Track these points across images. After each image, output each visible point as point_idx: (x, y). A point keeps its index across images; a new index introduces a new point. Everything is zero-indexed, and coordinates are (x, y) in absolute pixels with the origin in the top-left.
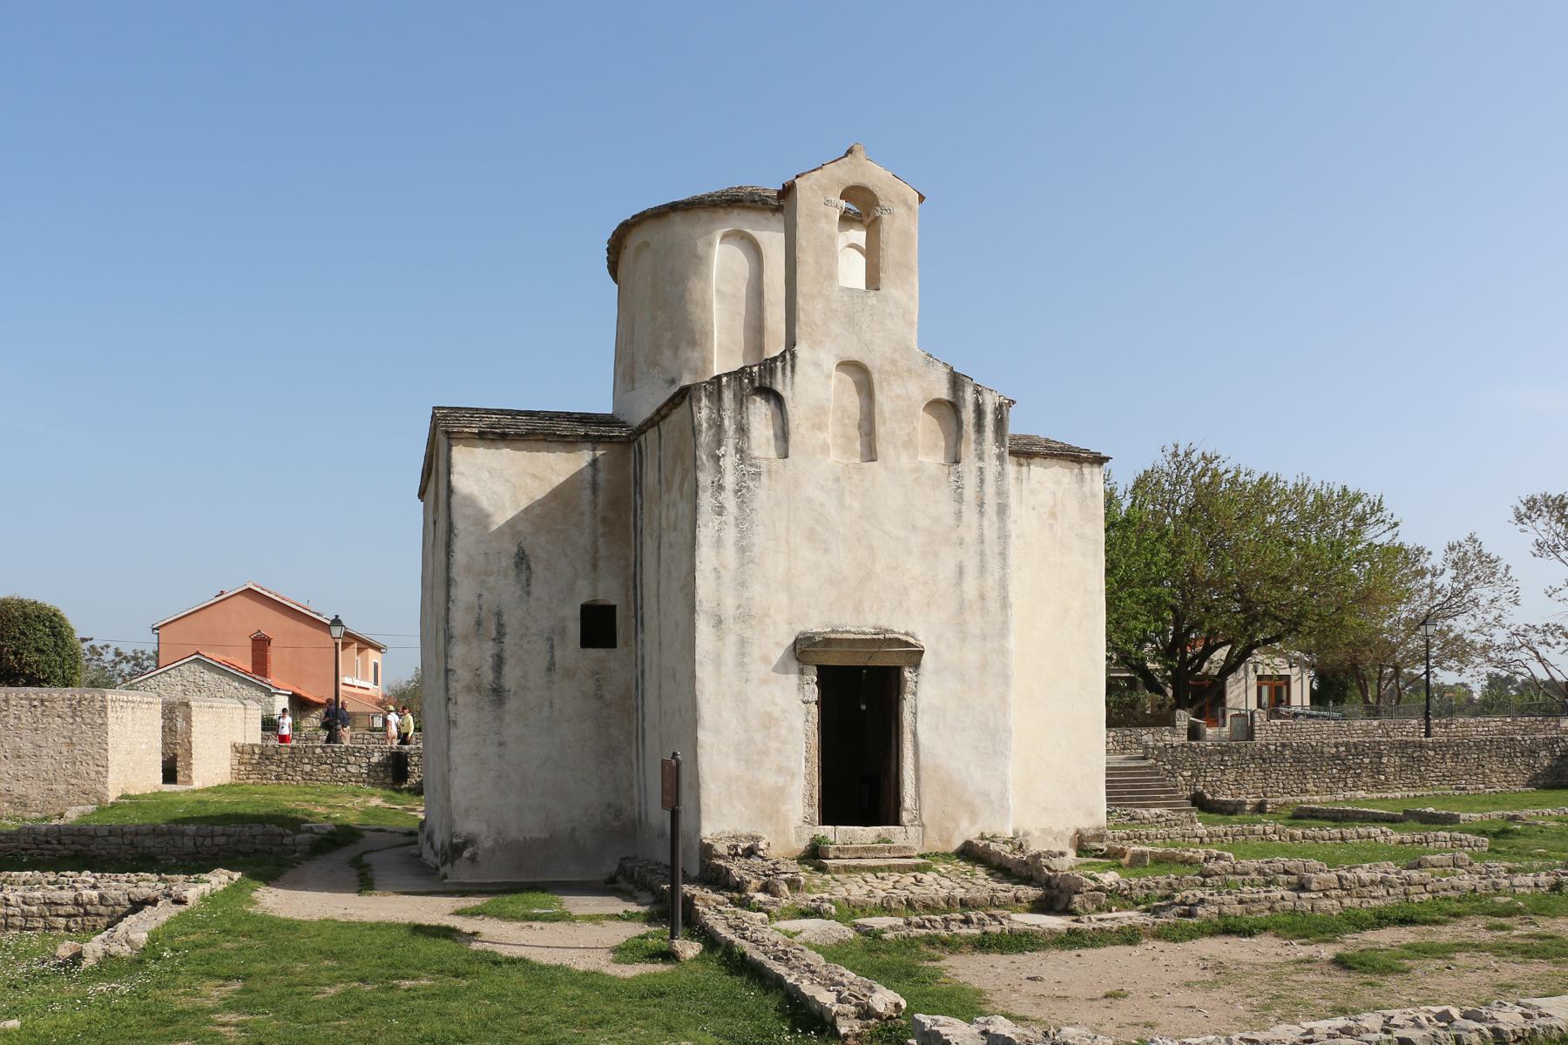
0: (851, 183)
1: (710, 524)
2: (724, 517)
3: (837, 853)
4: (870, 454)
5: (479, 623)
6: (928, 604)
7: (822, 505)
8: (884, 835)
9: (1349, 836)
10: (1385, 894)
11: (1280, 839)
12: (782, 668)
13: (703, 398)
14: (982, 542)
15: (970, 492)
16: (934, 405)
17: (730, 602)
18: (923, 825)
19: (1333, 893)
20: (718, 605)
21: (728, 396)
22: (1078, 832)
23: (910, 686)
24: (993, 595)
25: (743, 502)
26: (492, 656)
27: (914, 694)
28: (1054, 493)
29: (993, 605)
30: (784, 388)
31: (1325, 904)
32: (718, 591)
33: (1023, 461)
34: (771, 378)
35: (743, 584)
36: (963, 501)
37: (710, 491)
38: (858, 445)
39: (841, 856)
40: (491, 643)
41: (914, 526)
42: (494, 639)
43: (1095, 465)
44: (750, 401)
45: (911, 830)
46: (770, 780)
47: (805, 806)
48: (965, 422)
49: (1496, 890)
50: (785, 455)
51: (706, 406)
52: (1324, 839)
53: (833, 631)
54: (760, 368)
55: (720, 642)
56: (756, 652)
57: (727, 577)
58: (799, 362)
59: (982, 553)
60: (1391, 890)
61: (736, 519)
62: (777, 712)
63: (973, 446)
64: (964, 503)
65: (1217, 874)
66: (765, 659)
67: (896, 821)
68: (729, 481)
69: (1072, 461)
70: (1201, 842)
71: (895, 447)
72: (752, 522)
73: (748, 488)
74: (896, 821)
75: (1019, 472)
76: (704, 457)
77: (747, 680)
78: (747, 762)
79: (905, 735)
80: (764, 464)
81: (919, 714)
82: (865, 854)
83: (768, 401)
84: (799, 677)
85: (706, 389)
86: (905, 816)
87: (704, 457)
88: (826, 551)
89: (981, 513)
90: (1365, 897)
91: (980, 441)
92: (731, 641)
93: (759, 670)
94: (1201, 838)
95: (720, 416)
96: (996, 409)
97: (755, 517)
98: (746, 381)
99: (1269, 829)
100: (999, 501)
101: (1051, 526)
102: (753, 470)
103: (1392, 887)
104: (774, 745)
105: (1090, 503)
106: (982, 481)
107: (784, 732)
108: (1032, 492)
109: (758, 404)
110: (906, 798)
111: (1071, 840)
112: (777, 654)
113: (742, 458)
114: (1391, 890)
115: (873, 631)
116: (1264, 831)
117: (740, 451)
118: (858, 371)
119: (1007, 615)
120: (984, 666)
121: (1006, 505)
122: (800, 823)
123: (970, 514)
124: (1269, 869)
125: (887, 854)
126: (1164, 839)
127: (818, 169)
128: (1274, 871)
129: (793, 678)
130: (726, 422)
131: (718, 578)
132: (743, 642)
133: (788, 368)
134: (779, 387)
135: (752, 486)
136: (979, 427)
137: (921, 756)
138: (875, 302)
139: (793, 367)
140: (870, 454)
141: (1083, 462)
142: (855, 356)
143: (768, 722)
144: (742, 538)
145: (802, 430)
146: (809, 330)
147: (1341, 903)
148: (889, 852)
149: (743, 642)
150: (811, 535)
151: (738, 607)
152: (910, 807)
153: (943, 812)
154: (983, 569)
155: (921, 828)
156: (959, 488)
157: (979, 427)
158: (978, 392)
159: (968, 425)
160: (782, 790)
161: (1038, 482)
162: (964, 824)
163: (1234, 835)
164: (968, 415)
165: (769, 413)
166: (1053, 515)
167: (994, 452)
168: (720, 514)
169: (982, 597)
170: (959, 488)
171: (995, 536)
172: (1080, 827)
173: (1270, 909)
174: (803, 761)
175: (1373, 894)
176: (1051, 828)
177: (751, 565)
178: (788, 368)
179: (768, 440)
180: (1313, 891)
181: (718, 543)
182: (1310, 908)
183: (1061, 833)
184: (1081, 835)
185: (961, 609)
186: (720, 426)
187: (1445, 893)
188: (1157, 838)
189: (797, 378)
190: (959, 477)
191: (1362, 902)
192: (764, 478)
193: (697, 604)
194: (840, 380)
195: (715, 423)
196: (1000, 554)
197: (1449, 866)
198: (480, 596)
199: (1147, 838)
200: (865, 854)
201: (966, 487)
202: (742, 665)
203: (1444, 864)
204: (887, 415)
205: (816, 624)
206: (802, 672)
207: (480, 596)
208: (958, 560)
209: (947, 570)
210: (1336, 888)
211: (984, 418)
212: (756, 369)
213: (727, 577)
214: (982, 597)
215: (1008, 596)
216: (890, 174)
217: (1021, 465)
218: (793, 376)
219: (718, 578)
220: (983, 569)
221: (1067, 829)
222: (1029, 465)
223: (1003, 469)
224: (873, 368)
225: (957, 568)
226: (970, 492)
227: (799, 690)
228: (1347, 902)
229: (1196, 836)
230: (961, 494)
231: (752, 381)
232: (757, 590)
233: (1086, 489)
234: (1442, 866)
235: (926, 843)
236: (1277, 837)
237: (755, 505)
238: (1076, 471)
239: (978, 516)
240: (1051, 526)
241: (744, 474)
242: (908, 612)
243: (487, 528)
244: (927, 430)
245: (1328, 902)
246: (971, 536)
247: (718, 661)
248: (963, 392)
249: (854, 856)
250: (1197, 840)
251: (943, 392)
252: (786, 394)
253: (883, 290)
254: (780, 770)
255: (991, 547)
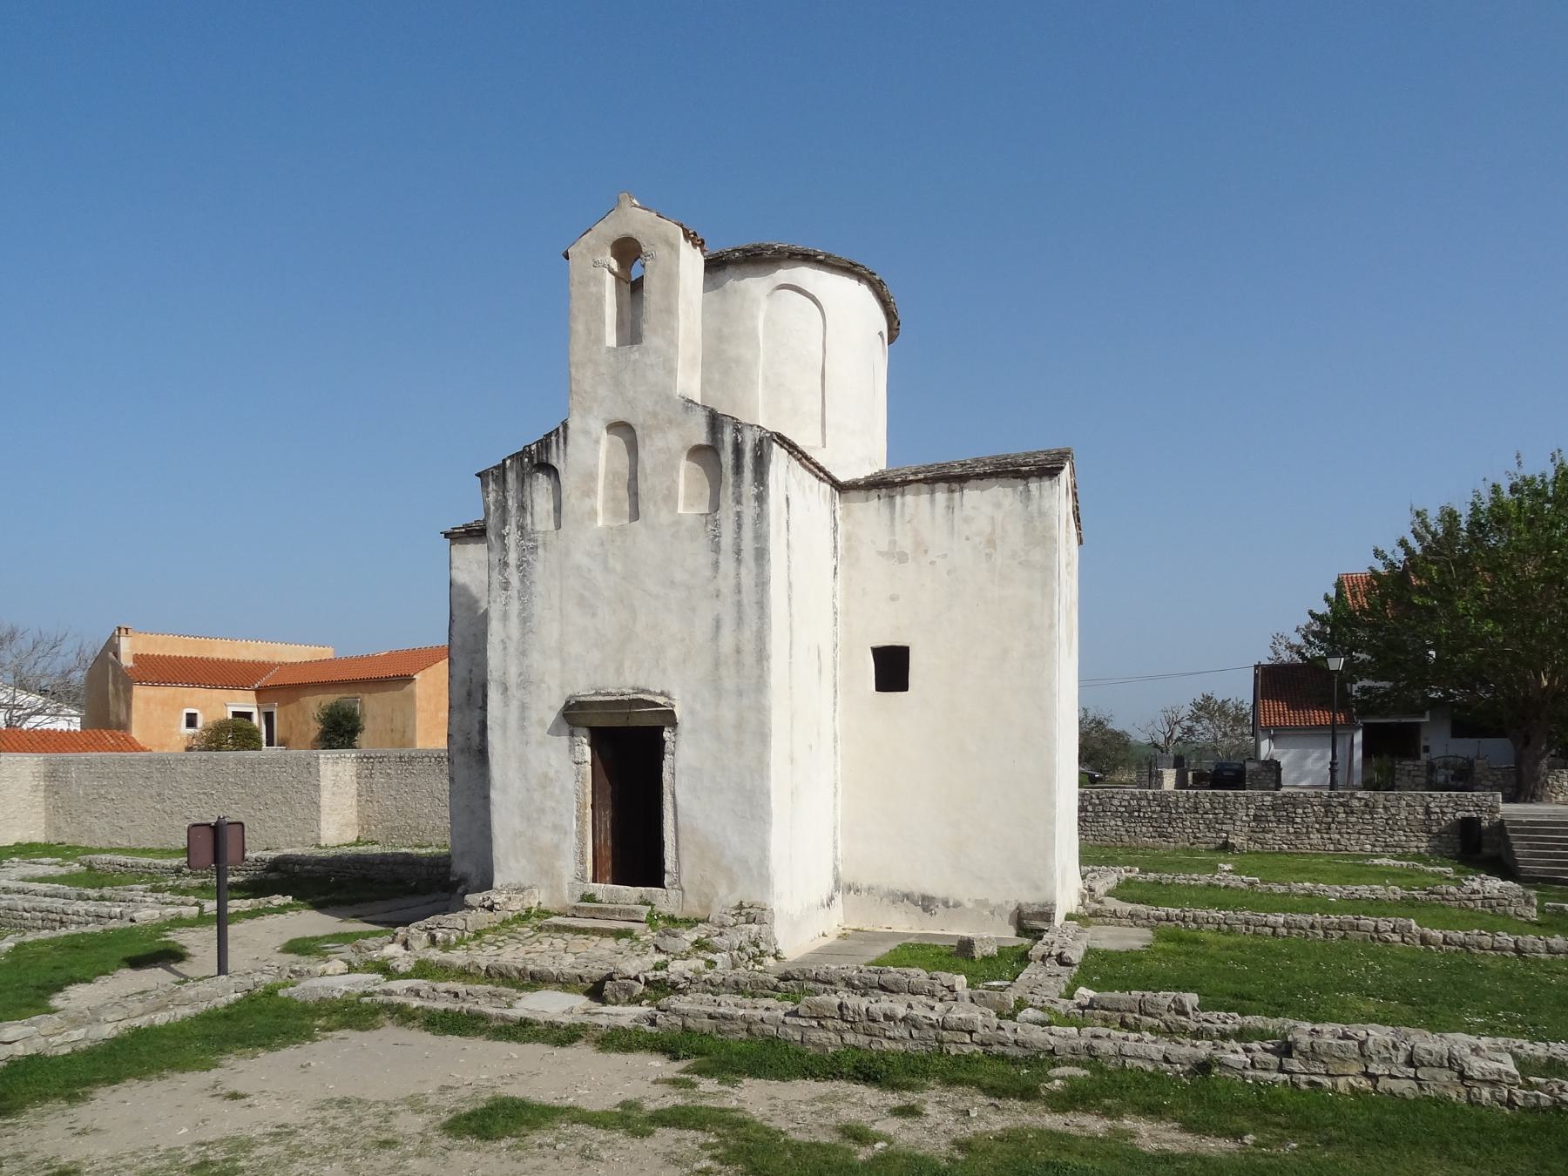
0: (617, 237)
1: (498, 599)
2: (509, 592)
3: (574, 912)
4: (635, 515)
5: (469, 694)
6: (684, 661)
7: (590, 570)
8: (647, 897)
9: (1529, 947)
10: (906, 1035)
11: (1403, 941)
12: (554, 731)
13: (491, 483)
14: (739, 592)
15: (727, 540)
16: (696, 452)
17: (513, 671)
18: (682, 889)
19: (830, 1023)
20: (504, 673)
21: (511, 477)
22: (1018, 908)
23: (669, 746)
24: (749, 648)
25: (524, 576)
26: (479, 722)
27: (673, 754)
28: (993, 518)
29: (749, 659)
30: (558, 462)
31: (817, 1036)
32: (505, 661)
33: (955, 486)
34: (547, 453)
35: (523, 653)
36: (720, 550)
37: (498, 569)
38: (627, 507)
39: (577, 915)
40: (478, 711)
41: (672, 582)
42: (480, 708)
43: (1044, 478)
44: (534, 478)
45: (673, 894)
46: (547, 838)
47: (576, 864)
48: (724, 466)
49: (1091, 1056)
50: (558, 526)
51: (493, 490)
52: (1481, 948)
53: (596, 694)
54: (537, 446)
55: (506, 708)
56: (534, 716)
57: (512, 649)
58: (570, 432)
59: (739, 604)
60: (915, 1032)
61: (519, 592)
62: (552, 774)
63: (730, 490)
64: (721, 552)
65: (794, 979)
66: (541, 722)
67: (659, 883)
68: (513, 557)
69: (1014, 478)
70: (1274, 933)
71: (655, 503)
72: (531, 594)
73: (527, 562)
74: (659, 883)
75: (950, 500)
76: (493, 538)
77: (527, 743)
78: (528, 819)
79: (664, 796)
80: (540, 537)
81: (676, 774)
82: (597, 915)
83: (549, 476)
84: (570, 739)
85: (493, 474)
86: (667, 879)
87: (493, 538)
88: (594, 615)
89: (739, 561)
90: (875, 1036)
91: (738, 484)
92: (514, 705)
93: (537, 732)
94: (1274, 928)
95: (505, 497)
96: (756, 445)
97: (533, 589)
98: (526, 460)
99: (1382, 925)
100: (756, 546)
101: (989, 556)
102: (531, 544)
103: (917, 1028)
104: (549, 804)
105: (1038, 524)
106: (740, 526)
107: (557, 791)
108: (967, 520)
109: (540, 480)
110: (666, 861)
111: (1011, 916)
112: (551, 717)
113: (522, 535)
114: (915, 1032)
115: (631, 691)
116: (1376, 927)
117: (521, 527)
118: (622, 429)
119: (763, 669)
120: (739, 726)
121: (764, 549)
122: (572, 880)
123: (727, 563)
124: (859, 980)
125: (617, 916)
126: (1219, 924)
127: (588, 231)
128: (865, 984)
129: (565, 740)
130: (510, 502)
131: (505, 648)
132: (523, 707)
133: (561, 440)
134: (553, 462)
135: (530, 559)
136: (738, 468)
137: (679, 818)
138: (637, 356)
139: (565, 439)
140: (635, 515)
141: (1028, 477)
142: (621, 417)
143: (545, 781)
144: (524, 609)
145: (573, 500)
146: (580, 399)
147: (842, 1038)
148: (620, 915)
149: (523, 707)
150: (582, 601)
151: (520, 675)
152: (670, 870)
153: (702, 877)
154: (740, 620)
155: (680, 892)
156: (716, 536)
157: (738, 468)
158: (738, 431)
159: (727, 468)
160: (557, 847)
161: (973, 508)
162: (723, 891)
163: (1325, 929)
164: (727, 457)
165: (550, 487)
166: (991, 543)
167: (752, 493)
168: (506, 589)
169: (738, 651)
170: (716, 536)
171: (753, 583)
172: (1023, 901)
173: (748, 1030)
174: (574, 819)
175: (887, 1033)
176: (987, 900)
177: (530, 634)
178: (561, 440)
179: (548, 512)
180: (801, 1017)
181: (505, 617)
182: (799, 1038)
183: (1000, 906)
184: (1020, 912)
185: (717, 664)
186: (504, 507)
187: (1002, 1049)
188: (1208, 922)
189: (569, 449)
190: (717, 526)
191: (871, 1042)
192: (540, 551)
193: (489, 673)
194: (612, 444)
195: (501, 504)
196: (757, 603)
197: (1132, 1012)
198: (471, 671)
199: (1194, 921)
200: (597, 915)
201: (723, 535)
202: (522, 728)
203: (1122, 1007)
204: (648, 471)
205: (583, 687)
206: (572, 734)
207: (471, 671)
208: (716, 613)
209: (702, 628)
210: (834, 1018)
211: (743, 457)
212: (534, 447)
213: (512, 649)
214: (738, 651)
215: (765, 648)
216: (655, 215)
217: (953, 491)
218: (565, 447)
219: (505, 648)
220: (740, 620)
221: (1007, 902)
222: (962, 490)
223: (762, 510)
224: (636, 425)
225: (714, 623)
226: (727, 540)
227: (570, 751)
228: (850, 1038)
229: (1266, 925)
230: (718, 542)
231: (531, 459)
232: (535, 658)
233: (1033, 507)
234: (1118, 1010)
235: (684, 908)
236: (1397, 938)
237: (535, 577)
238: (1021, 488)
239: (735, 564)
240: (989, 556)
241: (524, 550)
242: (664, 671)
243: (476, 612)
244: (686, 478)
245: (822, 1034)
246: (726, 586)
247: (504, 726)
248: (722, 433)
249: (589, 915)
250: (1268, 930)
251: (702, 438)
252: (560, 467)
253: (645, 343)
254: (555, 828)
255: (749, 598)
